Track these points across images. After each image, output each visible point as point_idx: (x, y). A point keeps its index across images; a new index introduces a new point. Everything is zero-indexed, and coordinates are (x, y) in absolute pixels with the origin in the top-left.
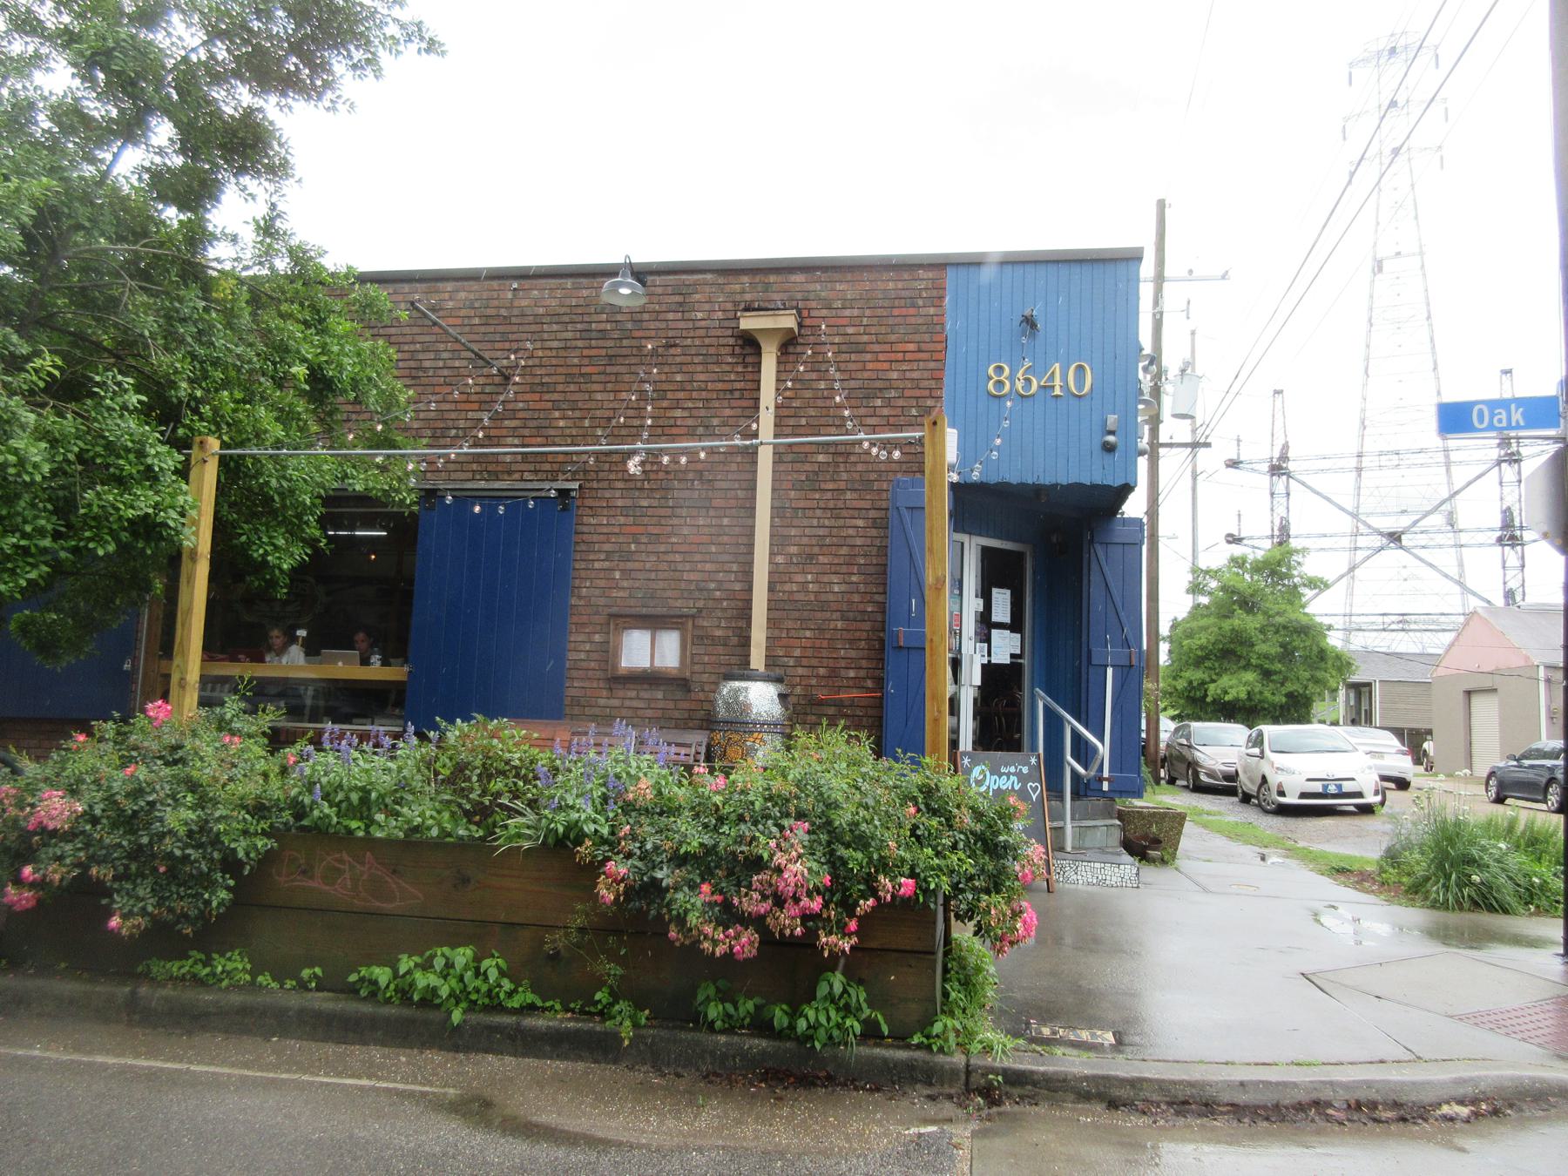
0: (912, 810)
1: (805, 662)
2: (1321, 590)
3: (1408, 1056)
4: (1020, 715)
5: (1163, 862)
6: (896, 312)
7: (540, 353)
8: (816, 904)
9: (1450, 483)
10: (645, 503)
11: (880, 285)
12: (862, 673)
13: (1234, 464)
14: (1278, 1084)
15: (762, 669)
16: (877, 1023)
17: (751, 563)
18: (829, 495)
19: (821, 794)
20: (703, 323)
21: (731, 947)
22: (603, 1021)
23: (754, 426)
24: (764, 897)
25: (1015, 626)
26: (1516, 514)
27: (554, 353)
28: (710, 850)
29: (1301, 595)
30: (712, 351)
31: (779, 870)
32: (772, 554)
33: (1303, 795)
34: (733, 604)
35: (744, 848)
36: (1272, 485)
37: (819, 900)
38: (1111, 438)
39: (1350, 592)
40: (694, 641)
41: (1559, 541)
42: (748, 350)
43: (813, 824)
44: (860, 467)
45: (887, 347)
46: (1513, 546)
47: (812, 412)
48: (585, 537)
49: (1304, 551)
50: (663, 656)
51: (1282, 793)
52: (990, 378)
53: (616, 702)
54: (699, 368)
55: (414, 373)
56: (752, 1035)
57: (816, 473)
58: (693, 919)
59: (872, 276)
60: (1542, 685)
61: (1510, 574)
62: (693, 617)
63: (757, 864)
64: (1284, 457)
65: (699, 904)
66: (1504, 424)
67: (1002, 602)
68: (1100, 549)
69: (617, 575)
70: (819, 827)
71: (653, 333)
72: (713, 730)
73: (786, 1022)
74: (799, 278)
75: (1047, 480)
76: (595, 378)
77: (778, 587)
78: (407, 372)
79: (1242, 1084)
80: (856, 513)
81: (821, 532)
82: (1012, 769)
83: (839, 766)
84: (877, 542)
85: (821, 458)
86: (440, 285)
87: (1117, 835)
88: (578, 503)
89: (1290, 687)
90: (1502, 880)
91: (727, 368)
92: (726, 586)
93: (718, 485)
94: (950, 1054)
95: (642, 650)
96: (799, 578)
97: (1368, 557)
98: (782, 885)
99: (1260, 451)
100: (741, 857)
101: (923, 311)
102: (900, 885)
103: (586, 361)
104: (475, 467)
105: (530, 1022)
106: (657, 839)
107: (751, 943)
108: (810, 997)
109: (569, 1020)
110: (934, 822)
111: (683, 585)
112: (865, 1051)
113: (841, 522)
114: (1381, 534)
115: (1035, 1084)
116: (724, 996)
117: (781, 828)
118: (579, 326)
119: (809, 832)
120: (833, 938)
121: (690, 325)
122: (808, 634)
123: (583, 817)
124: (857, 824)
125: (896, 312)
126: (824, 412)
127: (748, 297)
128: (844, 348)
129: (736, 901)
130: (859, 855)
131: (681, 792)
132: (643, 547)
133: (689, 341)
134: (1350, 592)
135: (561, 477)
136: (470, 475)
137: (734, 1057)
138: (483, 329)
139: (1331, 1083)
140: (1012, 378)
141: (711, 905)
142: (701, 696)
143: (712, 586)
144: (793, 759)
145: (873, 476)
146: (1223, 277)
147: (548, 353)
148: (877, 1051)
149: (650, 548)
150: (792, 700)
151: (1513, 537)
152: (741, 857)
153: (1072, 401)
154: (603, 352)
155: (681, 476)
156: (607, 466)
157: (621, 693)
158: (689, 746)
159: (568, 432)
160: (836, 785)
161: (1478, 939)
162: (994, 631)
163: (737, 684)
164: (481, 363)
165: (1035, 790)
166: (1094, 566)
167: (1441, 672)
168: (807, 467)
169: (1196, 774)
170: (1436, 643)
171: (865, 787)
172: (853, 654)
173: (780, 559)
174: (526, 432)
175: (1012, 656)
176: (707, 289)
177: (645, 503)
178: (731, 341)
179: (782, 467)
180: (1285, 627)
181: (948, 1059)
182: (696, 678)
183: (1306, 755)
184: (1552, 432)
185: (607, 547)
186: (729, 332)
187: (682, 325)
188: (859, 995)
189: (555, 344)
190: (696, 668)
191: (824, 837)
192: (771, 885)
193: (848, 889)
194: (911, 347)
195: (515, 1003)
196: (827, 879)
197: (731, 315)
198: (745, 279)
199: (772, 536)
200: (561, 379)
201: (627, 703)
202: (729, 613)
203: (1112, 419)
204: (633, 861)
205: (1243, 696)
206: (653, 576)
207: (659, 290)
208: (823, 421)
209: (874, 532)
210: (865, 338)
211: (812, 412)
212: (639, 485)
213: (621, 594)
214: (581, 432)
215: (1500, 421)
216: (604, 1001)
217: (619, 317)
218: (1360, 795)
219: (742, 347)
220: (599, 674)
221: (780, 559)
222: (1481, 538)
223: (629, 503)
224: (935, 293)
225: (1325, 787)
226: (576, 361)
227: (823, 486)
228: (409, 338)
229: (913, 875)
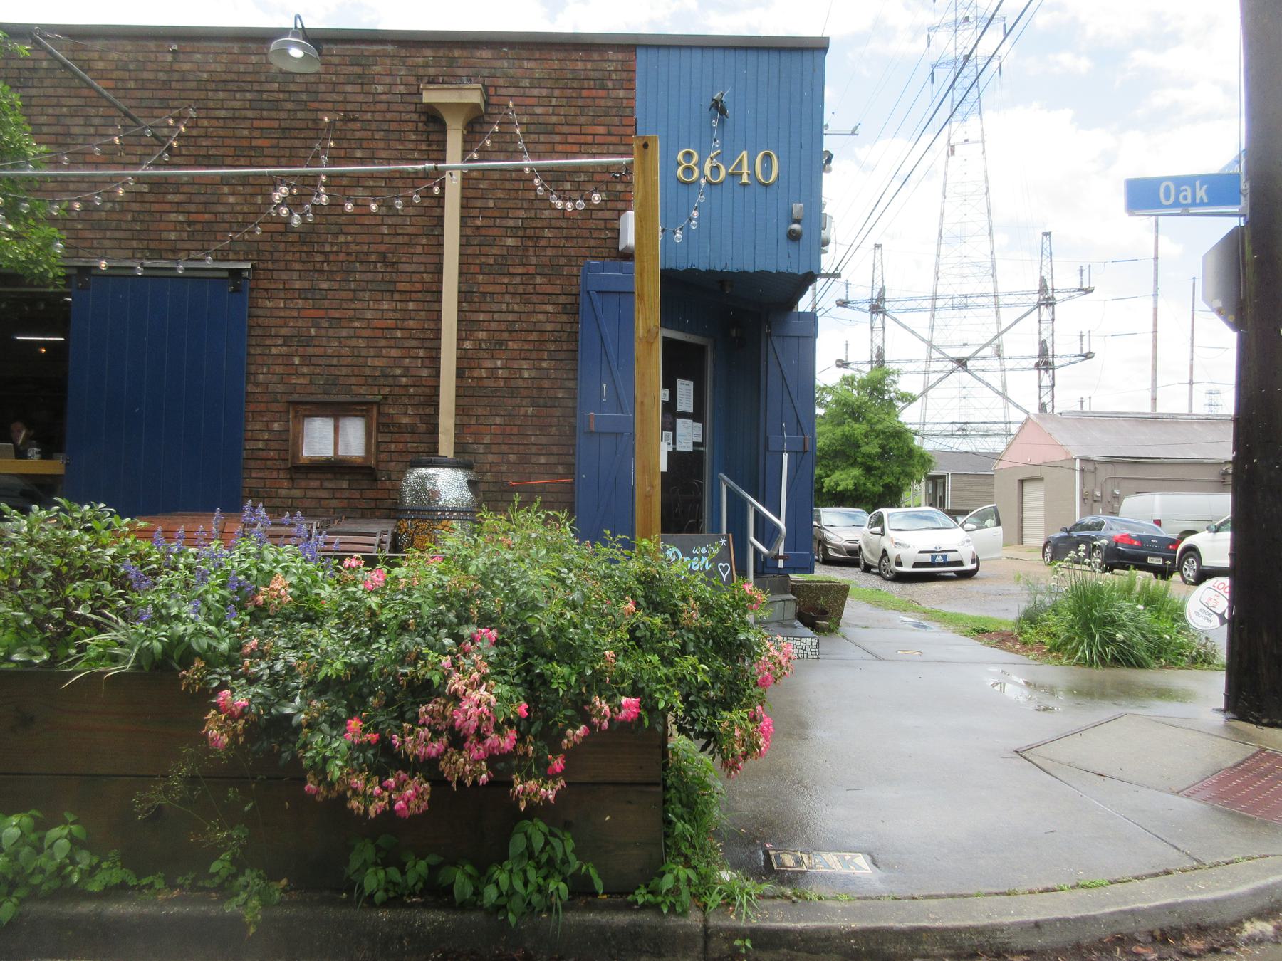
0: (631, 606)
1: (495, 448)
2: (910, 403)
3: (1189, 864)
4: (700, 501)
5: (831, 631)
6: (584, 93)
7: (206, 123)
8: (506, 742)
9: (999, 323)
10: (324, 286)
11: (569, 65)
12: (553, 459)
13: (843, 303)
14: (1077, 920)
15: (450, 455)
16: (588, 877)
17: (438, 349)
18: (518, 280)
19: (513, 590)
20: (384, 97)
21: (392, 802)
22: (222, 900)
23: (436, 190)
24: (436, 734)
25: (697, 416)
26: (1049, 345)
27: (221, 123)
28: (359, 671)
29: (895, 407)
30: (394, 126)
31: (456, 698)
32: (459, 339)
33: (916, 565)
34: (420, 390)
35: (408, 670)
37: (512, 734)
38: (796, 226)
39: (924, 408)
40: (379, 429)
41: (1232, 318)
42: (431, 127)
43: (502, 631)
44: (549, 252)
45: (577, 129)
46: (1046, 370)
47: (500, 194)
48: (260, 321)
49: (898, 373)
50: (347, 445)
51: (899, 564)
52: (679, 164)
53: (298, 493)
54: (381, 144)
55: (60, 139)
56: (425, 906)
57: (503, 256)
58: (335, 770)
59: (561, 55)
60: (1078, 474)
61: (1044, 391)
62: (378, 404)
63: (424, 690)
64: (881, 298)
65: (344, 748)
66: (1189, 201)
67: (685, 389)
68: (777, 342)
69: (297, 361)
70: (511, 636)
71: (330, 106)
72: (399, 519)
73: (469, 890)
74: (485, 53)
75: (735, 267)
76: (266, 152)
77: (467, 373)
78: (52, 138)
79: (1037, 925)
80: (546, 298)
81: (511, 317)
82: (704, 551)
83: (536, 558)
84: (568, 328)
85: (510, 242)
86: (89, 43)
87: (792, 608)
88: (253, 284)
89: (887, 479)
90: (1138, 637)
91: (411, 146)
92: (413, 372)
93: (402, 267)
94: (684, 913)
95: (321, 439)
96: (488, 364)
97: (941, 379)
98: (459, 718)
99: (862, 292)
100: (402, 680)
101: (613, 94)
102: (620, 707)
103: (257, 133)
104: (134, 244)
105: (115, 909)
106: (291, 657)
107: (418, 796)
108: (502, 857)
109: (172, 902)
110: (657, 620)
111: (368, 371)
112: (574, 918)
113: (530, 308)
114: (952, 359)
115: (791, 946)
116: (389, 859)
117: (459, 639)
118: (248, 96)
119: (497, 643)
120: (532, 784)
121: (370, 98)
122: (498, 420)
123: (191, 628)
124: (562, 629)
125: (584, 93)
126: (512, 194)
127: (432, 71)
128: (532, 128)
129: (396, 740)
130: (565, 670)
131: (326, 592)
132: (323, 332)
133: (369, 116)
134: (924, 408)
135: (231, 256)
136: (130, 253)
137: (401, 939)
138: (139, 94)
139: (1132, 912)
140: (700, 164)
141: (362, 747)
142: (388, 485)
143: (398, 372)
144: (476, 545)
145: (563, 261)
146: (853, 133)
147: (214, 123)
148: (590, 916)
149: (331, 332)
150: (483, 487)
151: (1046, 363)
152: (402, 680)
153: (761, 190)
154: (276, 124)
155: (363, 257)
156: (282, 246)
157: (303, 484)
158: (374, 535)
159: (238, 208)
160: (533, 579)
161: (1127, 692)
162: (679, 421)
163: (424, 470)
164: (129, 122)
165: (725, 570)
166: (771, 356)
167: (1002, 465)
168: (495, 251)
169: (825, 550)
170: (998, 445)
171: (571, 578)
172: (544, 440)
173: (468, 345)
174: (192, 208)
175: (695, 444)
176: (388, 61)
177: (324, 286)
178: (415, 117)
179: (469, 251)
180: (884, 433)
181: (682, 921)
182: (382, 466)
183: (911, 533)
184: (1235, 209)
185: (284, 331)
186: (412, 108)
187: (360, 98)
188: (565, 846)
189: (222, 114)
190: (383, 456)
191: (517, 650)
192: (445, 718)
193: (550, 717)
194: (601, 130)
195: (95, 887)
196: (522, 708)
197: (414, 89)
198: (428, 52)
199: (459, 321)
200: (230, 151)
201: (310, 493)
202: (416, 400)
203: (797, 207)
204: (256, 690)
205: (851, 487)
206: (335, 361)
207: (336, 60)
208: (511, 204)
209: (564, 318)
210: (554, 119)
211: (500, 194)
212: (318, 266)
213: (301, 381)
214: (252, 209)
215: (1185, 198)
216: (224, 873)
217: (292, 87)
218: (960, 563)
219: (425, 123)
220: (280, 464)
221: (468, 345)
222: (1024, 363)
223: (307, 285)
224: (624, 75)
225: (934, 558)
226: (246, 133)
227: (512, 270)
228: (54, 101)
229: (635, 691)
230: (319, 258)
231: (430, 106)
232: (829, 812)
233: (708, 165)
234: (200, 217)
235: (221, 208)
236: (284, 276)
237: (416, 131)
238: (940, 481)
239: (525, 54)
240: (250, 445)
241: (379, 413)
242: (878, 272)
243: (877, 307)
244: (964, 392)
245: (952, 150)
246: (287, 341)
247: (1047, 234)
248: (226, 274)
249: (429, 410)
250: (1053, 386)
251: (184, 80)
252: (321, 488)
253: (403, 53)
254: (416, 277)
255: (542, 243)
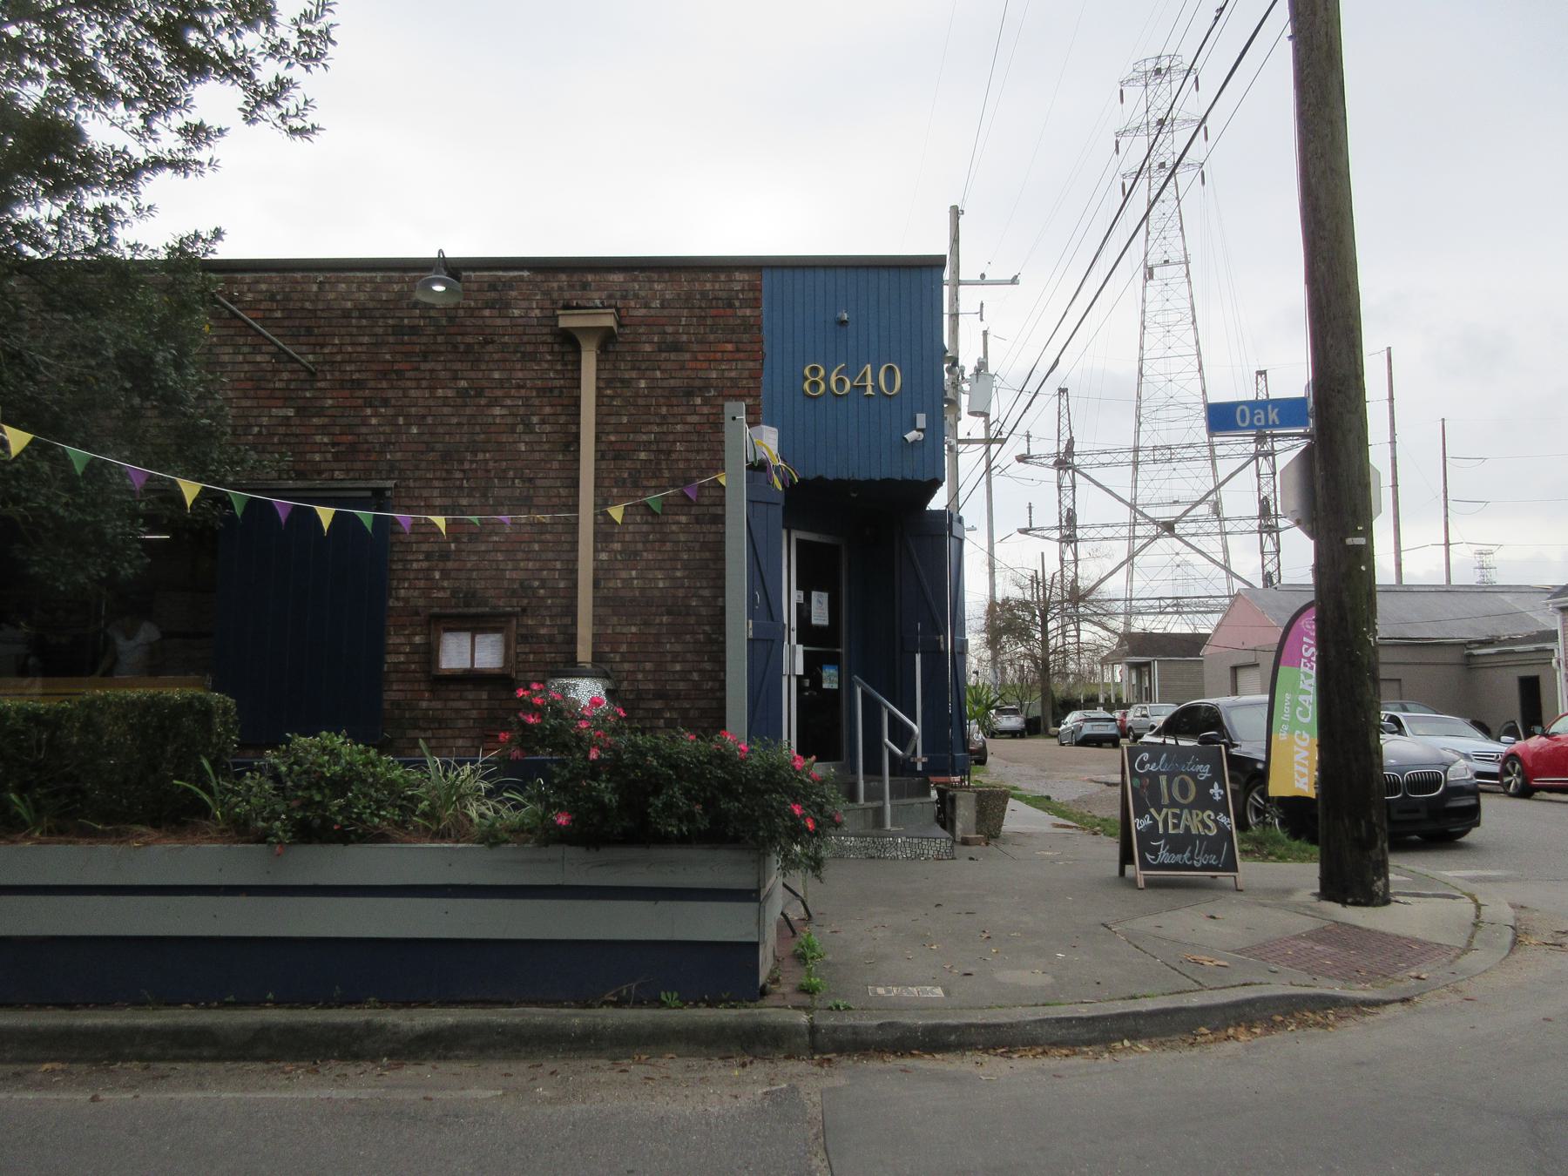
7: (350, 349)
9: (1215, 475)
13: (1022, 459)
32: (596, 551)
36: (1059, 478)
40: (519, 641)
52: (806, 379)
61: (1268, 558)
64: (1069, 451)
85: (643, 456)
86: (239, 276)
91: (545, 366)
93: (538, 483)
96: (624, 574)
97: (1145, 546)
101: (739, 313)
103: (398, 357)
111: (506, 584)
121: (507, 322)
140: (826, 379)
143: (536, 584)
170: (1205, 625)
172: (678, 648)
174: (337, 430)
185: (425, 547)
198: (563, 277)
230: (458, 475)
231: (565, 330)
232: (843, 879)
233: (833, 379)
234: (345, 439)
235: (364, 430)
236: (425, 493)
237: (552, 352)
238: (1145, 669)
239: (655, 276)
240: (391, 659)
241: (518, 626)
242: (1064, 421)
243: (1064, 463)
244: (1178, 559)
245: (1149, 274)
246: (428, 556)
247: (1262, 373)
248: (369, 494)
249: (568, 621)
250: (1278, 551)
251: (329, 309)
252: (461, 699)
253: (540, 278)
254: (553, 492)
255: (674, 456)
